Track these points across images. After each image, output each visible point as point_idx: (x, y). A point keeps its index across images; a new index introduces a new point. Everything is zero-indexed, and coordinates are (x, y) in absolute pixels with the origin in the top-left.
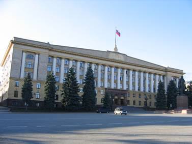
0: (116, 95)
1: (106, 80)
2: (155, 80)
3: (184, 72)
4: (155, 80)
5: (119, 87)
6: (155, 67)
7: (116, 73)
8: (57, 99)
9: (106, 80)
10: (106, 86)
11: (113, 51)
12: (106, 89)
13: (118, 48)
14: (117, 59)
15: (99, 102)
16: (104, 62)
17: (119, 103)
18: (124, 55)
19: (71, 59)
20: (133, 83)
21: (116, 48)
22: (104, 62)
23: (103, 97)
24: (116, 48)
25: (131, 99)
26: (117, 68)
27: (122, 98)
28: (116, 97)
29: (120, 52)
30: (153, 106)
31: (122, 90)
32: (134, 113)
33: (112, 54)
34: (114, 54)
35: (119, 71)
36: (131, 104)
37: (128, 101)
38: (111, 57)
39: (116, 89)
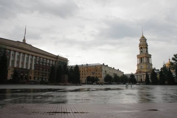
0: (22, 72)
1: (20, 63)
2: (32, 60)
3: (68, 60)
4: (32, 60)
5: (25, 67)
6: (50, 55)
7: (23, 58)
8: (30, 79)
9: (20, 63)
10: (15, 66)
11: (22, 41)
12: (15, 68)
13: (26, 40)
14: (25, 48)
15: (9, 76)
16: (37, 55)
17: (24, 78)
18: (31, 45)
19: (17, 51)
20: (30, 64)
21: (24, 40)
22: (37, 55)
23: (12, 73)
24: (24, 40)
25: (32, 75)
26: (24, 54)
27: (26, 75)
28: (22, 74)
29: (27, 43)
30: (48, 82)
31: (27, 69)
32: (59, 85)
33: (21, 44)
34: (23, 44)
35: (26, 56)
36: (32, 79)
37: (31, 77)
38: (21, 46)
39: (22, 68)
